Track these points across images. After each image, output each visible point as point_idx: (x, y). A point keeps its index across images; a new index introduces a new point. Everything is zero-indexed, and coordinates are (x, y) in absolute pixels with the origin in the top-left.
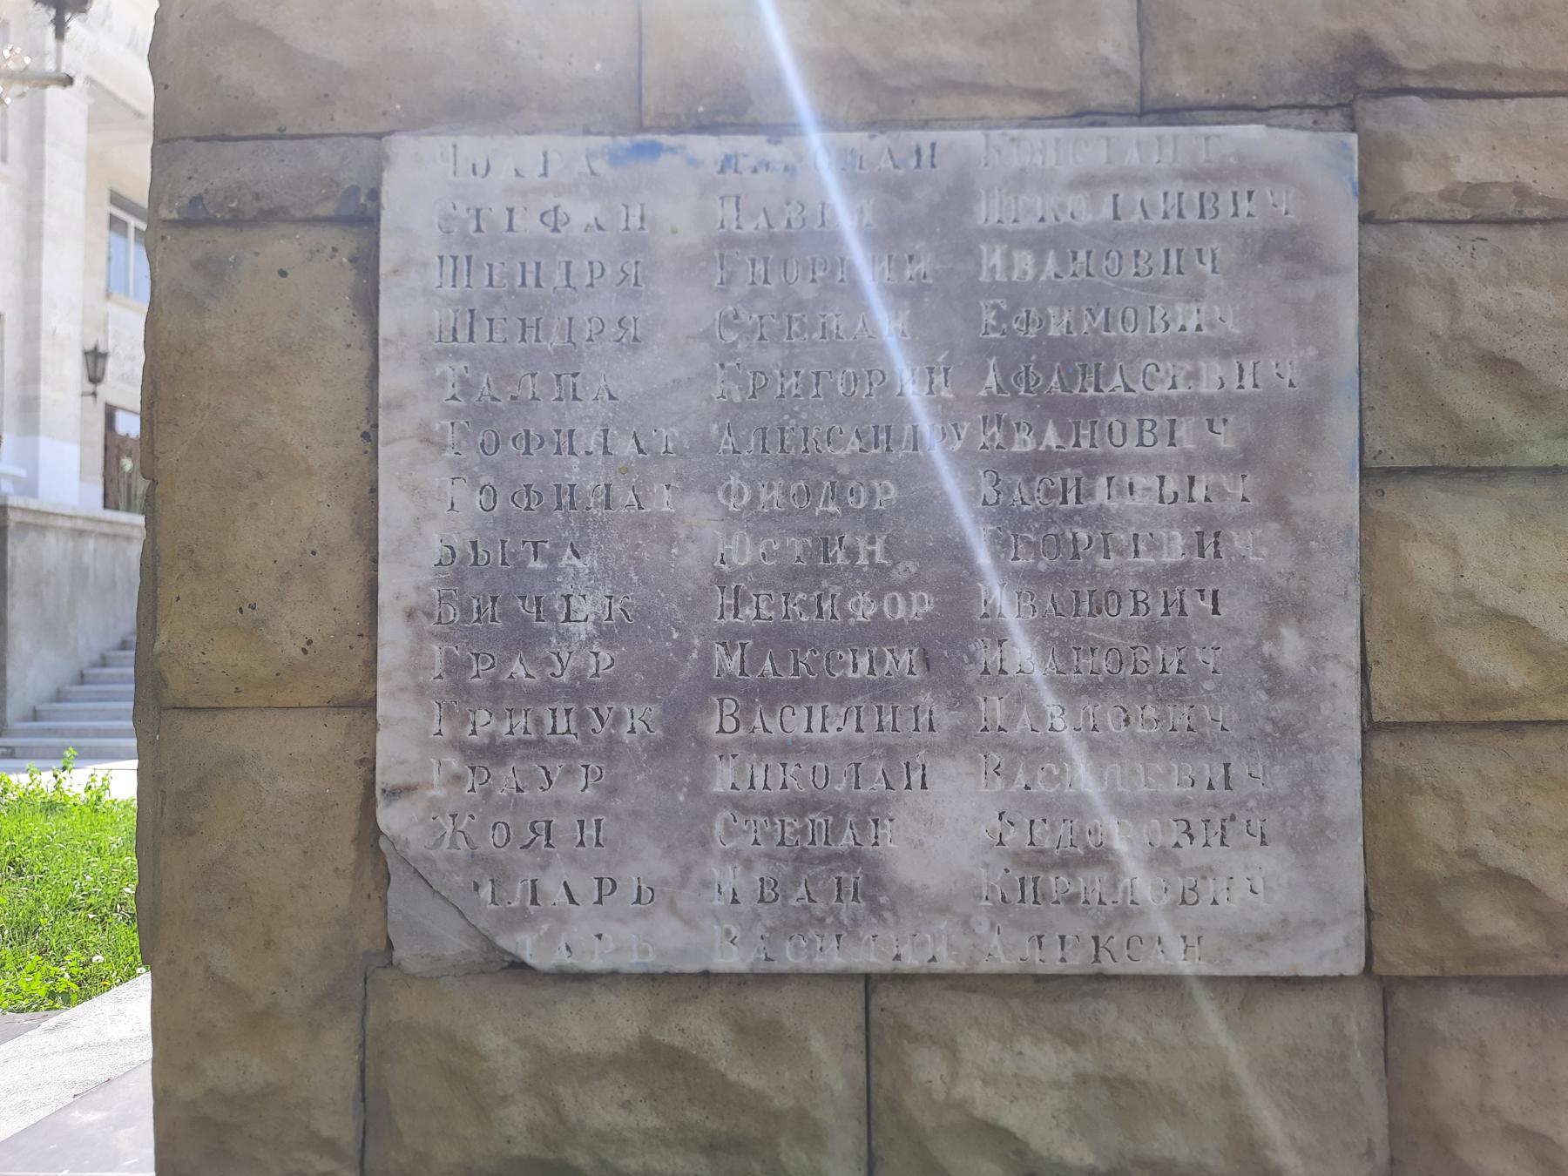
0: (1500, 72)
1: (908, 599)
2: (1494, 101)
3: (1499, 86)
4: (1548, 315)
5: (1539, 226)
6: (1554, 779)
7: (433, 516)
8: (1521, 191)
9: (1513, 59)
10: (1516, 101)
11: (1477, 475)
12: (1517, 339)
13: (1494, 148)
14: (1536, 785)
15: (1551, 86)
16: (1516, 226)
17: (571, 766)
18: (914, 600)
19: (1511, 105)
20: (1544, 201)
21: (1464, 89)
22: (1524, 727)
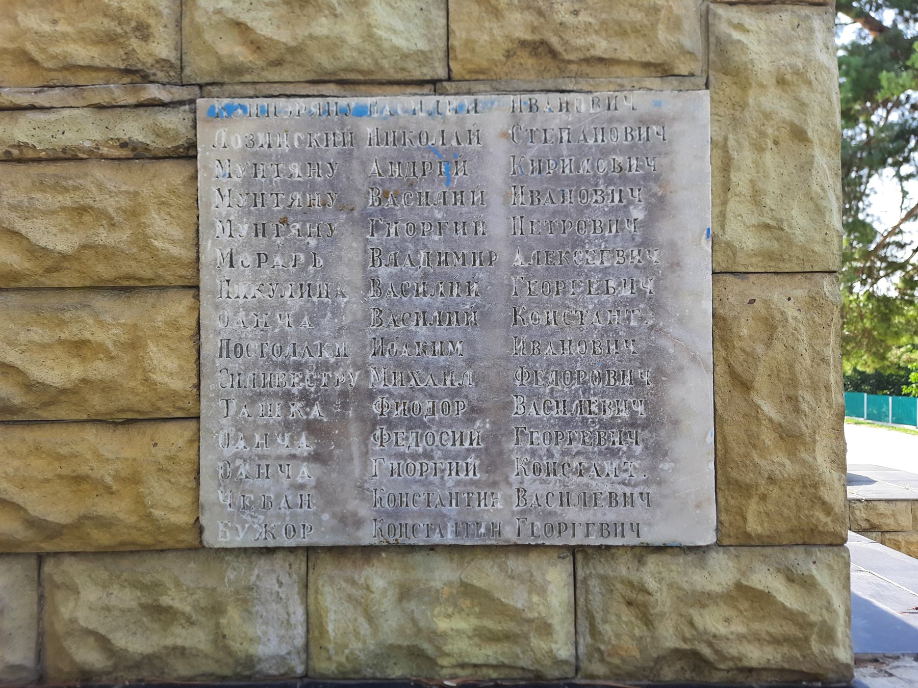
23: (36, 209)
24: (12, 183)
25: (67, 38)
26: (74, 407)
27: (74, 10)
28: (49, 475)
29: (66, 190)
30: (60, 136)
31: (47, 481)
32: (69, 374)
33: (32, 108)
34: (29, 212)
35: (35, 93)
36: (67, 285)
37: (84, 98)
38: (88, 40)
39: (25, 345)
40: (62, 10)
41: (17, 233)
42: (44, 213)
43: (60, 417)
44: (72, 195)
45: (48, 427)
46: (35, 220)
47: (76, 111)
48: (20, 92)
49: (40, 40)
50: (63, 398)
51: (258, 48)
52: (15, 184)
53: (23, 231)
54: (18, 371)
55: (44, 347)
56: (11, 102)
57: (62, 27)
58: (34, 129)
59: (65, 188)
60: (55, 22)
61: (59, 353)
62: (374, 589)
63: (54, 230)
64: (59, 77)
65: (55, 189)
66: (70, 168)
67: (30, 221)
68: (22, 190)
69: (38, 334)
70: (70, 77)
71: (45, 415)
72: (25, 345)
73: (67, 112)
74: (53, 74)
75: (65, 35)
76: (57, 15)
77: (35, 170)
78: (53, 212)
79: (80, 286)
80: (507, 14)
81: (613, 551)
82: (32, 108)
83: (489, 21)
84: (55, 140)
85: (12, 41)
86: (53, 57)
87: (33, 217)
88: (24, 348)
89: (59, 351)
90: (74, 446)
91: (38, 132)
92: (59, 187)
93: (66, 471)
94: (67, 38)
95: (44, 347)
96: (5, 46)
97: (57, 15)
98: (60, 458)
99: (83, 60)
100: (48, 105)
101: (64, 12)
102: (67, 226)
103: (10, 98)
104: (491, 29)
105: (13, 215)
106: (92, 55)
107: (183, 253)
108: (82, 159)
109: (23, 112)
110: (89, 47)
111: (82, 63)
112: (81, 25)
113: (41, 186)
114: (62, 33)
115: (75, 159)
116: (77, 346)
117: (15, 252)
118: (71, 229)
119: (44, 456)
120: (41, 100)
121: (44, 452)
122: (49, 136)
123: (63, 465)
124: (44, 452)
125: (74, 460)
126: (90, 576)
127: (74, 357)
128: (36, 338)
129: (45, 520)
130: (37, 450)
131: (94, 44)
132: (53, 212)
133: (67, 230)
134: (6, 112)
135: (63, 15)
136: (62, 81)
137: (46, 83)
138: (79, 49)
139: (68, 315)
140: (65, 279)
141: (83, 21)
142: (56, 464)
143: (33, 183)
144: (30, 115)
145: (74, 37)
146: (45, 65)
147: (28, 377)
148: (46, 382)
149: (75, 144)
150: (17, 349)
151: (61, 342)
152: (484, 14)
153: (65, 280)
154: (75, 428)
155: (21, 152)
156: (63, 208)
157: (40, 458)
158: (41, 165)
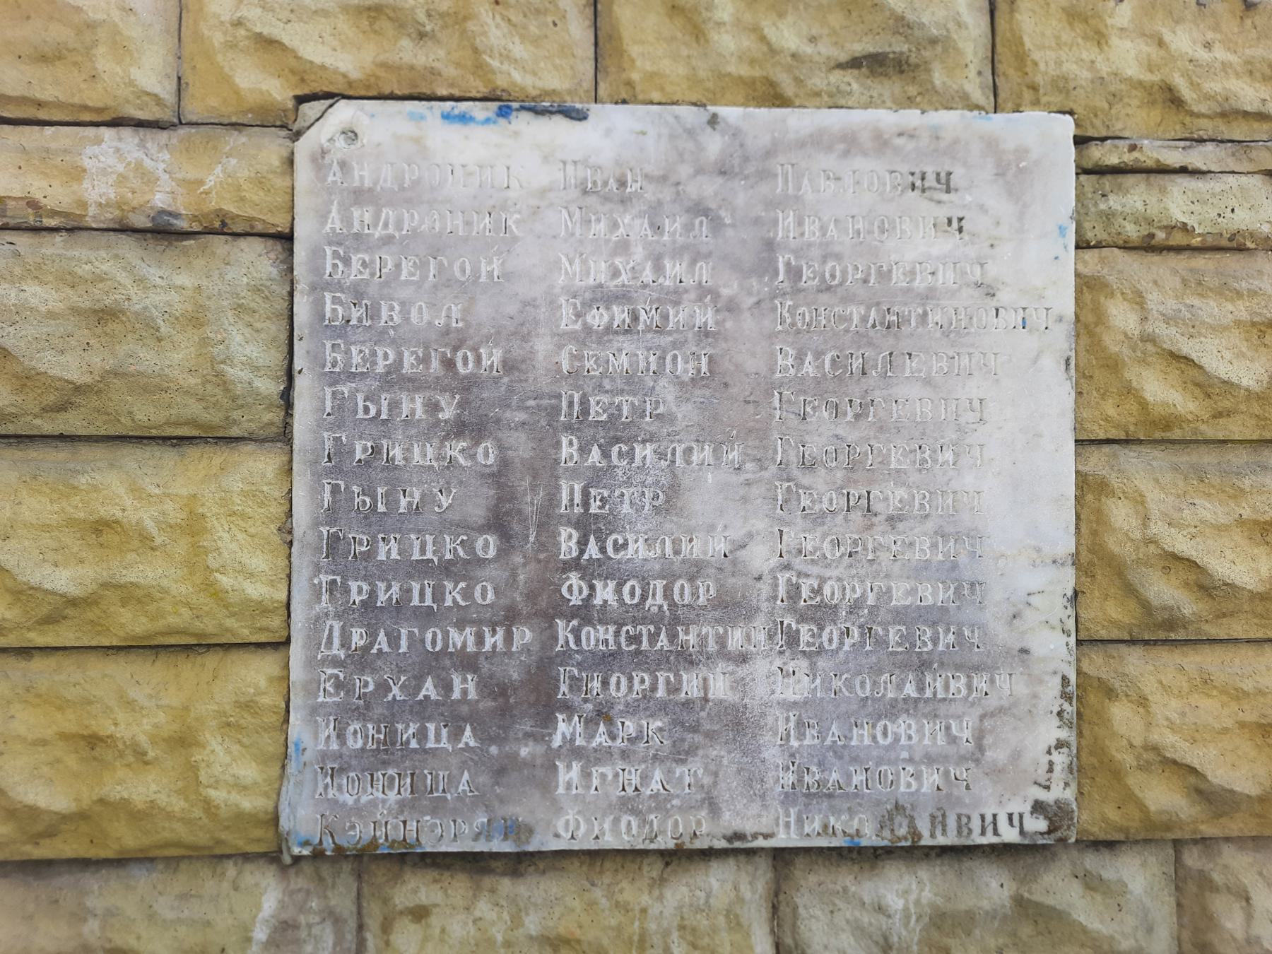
0: (40, 104)
1: (630, 679)
2: (36, 128)
3: (43, 115)
4: (43, 309)
5: (64, 234)
6: (39, 696)
7: (722, 641)
8: (33, 204)
9: (47, 93)
10: (53, 129)
11: (6, 441)
12: (11, 329)
13: (20, 168)
14: (26, 701)
15: (87, 117)
16: (44, 233)
17: (346, 921)
18: (636, 681)
19: (49, 131)
20: (54, 213)
21: (11, 116)
22: (33, 652)
23: (1203, 323)
24: (1155, 282)
25: (1230, 71)
26: (1256, 621)
27: (1236, 30)
28: (1229, 723)
29: (1239, 294)
30: (1228, 214)
31: (1225, 731)
32: (1258, 571)
33: (1183, 170)
34: (1193, 327)
35: (1184, 148)
36: (1237, 438)
37: (1251, 160)
38: (1258, 75)
39: (1196, 527)
40: (1216, 28)
41: (1187, 360)
42: (1214, 329)
43: (1235, 635)
44: (1248, 304)
45: (1217, 647)
46: (1202, 339)
47: (1244, 179)
48: (1165, 147)
49: (1194, 72)
50: (70, 612)
51: (179, 58)
52: (1159, 282)
53: (1194, 356)
54: (1192, 564)
55: (1219, 529)
56: (1158, 161)
57: (1220, 53)
58: (1193, 203)
59: (1238, 292)
60: (1208, 46)
61: (1237, 538)
62: (892, 911)
63: (1228, 355)
64: (1206, 127)
65: (1221, 294)
66: (1231, 262)
67: (1197, 340)
68: (1170, 292)
69: (1209, 510)
70: (1223, 128)
71: (1213, 631)
72: (1196, 527)
73: (1231, 179)
74: (1204, 123)
75: (1225, 66)
76: (1210, 35)
77: (1181, 263)
78: (1226, 328)
79: (1255, 438)
80: (1115, 40)
81: (1208, 842)
82: (1183, 170)
83: (1087, 50)
84: (1224, 220)
85: (1151, 71)
86: (1208, 97)
87: (1200, 334)
88: (1194, 530)
89: (1238, 537)
90: (1258, 679)
91: (1197, 208)
92: (1226, 291)
93: (1250, 717)
94: (1230, 71)
95: (1219, 529)
96: (1142, 77)
97: (1210, 35)
98: (1239, 695)
99: (1251, 104)
100: (1204, 168)
101: (1221, 32)
102: (1244, 350)
103: (1155, 155)
104: (1093, 62)
105: (1173, 330)
106: (1262, 97)
107: (270, 387)
108: (1248, 249)
109: (1173, 177)
110: (1258, 85)
111: (1249, 109)
112: (1248, 52)
113: (1198, 285)
114: (1223, 62)
115: (1241, 249)
116: (97, 529)
117: (1173, 386)
118: (1249, 354)
119: (1215, 692)
120: (1196, 157)
121: (1215, 687)
122: (1213, 215)
123: (1246, 707)
124: (1215, 687)
125: (1262, 700)
126: (1260, 874)
127: (1258, 545)
128: (1208, 516)
129: (1232, 792)
130: (1205, 683)
131: (1264, 80)
132: (1226, 328)
133: (1244, 355)
134: (1138, 175)
135: (1218, 36)
136: (1210, 133)
137: (1188, 135)
138: (1244, 86)
139: (1246, 483)
140: (72, 422)
141: (1251, 47)
142: (1234, 706)
143: (1185, 282)
144: (1184, 181)
145: (1239, 69)
146: (1195, 109)
147: (1211, 576)
148: (1237, 582)
149: (1251, 227)
150: (1185, 533)
151: (1241, 521)
152: (1080, 40)
153: (1235, 429)
154: (1248, 652)
155: (1169, 234)
156: (1238, 323)
157: (1209, 696)
158: (1181, 257)
